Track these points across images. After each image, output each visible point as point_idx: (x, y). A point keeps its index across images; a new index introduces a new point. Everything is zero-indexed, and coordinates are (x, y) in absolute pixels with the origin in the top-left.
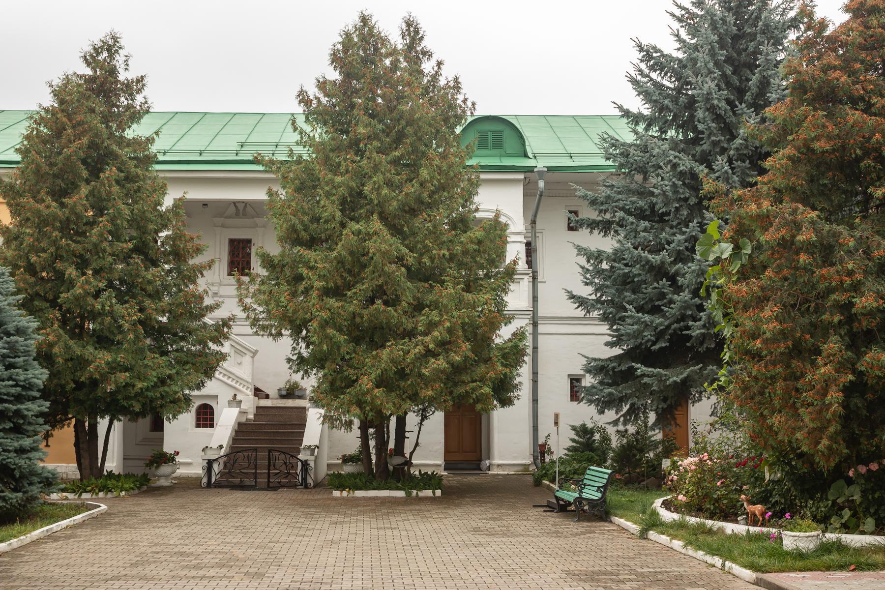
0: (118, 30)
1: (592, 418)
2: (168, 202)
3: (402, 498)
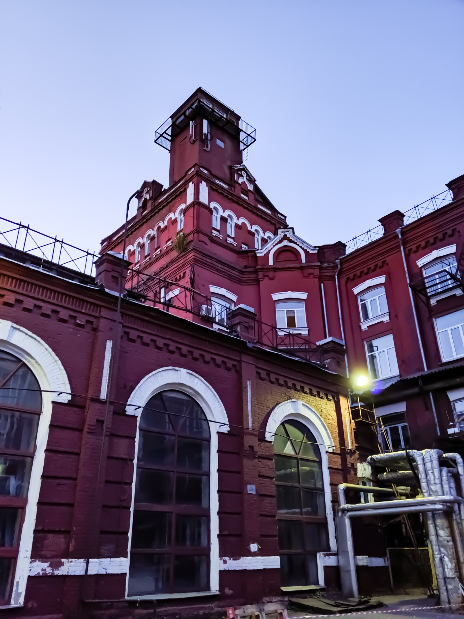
0: (216, 432)
1: (228, 567)
2: (433, 302)
3: (386, 276)
